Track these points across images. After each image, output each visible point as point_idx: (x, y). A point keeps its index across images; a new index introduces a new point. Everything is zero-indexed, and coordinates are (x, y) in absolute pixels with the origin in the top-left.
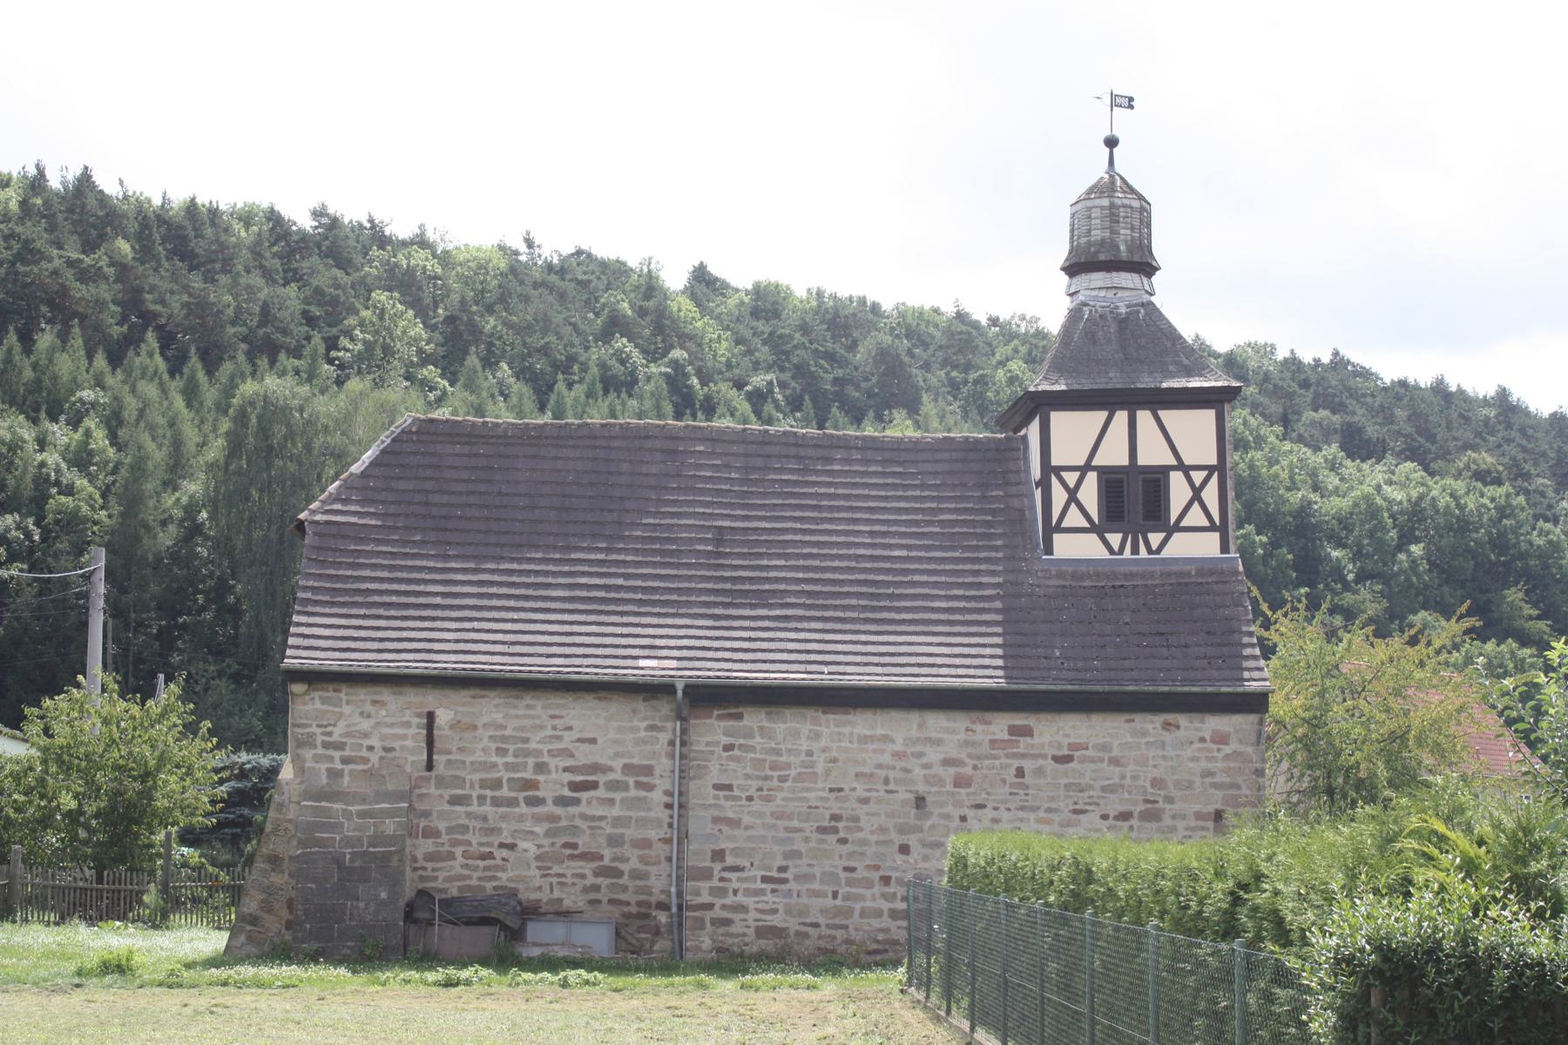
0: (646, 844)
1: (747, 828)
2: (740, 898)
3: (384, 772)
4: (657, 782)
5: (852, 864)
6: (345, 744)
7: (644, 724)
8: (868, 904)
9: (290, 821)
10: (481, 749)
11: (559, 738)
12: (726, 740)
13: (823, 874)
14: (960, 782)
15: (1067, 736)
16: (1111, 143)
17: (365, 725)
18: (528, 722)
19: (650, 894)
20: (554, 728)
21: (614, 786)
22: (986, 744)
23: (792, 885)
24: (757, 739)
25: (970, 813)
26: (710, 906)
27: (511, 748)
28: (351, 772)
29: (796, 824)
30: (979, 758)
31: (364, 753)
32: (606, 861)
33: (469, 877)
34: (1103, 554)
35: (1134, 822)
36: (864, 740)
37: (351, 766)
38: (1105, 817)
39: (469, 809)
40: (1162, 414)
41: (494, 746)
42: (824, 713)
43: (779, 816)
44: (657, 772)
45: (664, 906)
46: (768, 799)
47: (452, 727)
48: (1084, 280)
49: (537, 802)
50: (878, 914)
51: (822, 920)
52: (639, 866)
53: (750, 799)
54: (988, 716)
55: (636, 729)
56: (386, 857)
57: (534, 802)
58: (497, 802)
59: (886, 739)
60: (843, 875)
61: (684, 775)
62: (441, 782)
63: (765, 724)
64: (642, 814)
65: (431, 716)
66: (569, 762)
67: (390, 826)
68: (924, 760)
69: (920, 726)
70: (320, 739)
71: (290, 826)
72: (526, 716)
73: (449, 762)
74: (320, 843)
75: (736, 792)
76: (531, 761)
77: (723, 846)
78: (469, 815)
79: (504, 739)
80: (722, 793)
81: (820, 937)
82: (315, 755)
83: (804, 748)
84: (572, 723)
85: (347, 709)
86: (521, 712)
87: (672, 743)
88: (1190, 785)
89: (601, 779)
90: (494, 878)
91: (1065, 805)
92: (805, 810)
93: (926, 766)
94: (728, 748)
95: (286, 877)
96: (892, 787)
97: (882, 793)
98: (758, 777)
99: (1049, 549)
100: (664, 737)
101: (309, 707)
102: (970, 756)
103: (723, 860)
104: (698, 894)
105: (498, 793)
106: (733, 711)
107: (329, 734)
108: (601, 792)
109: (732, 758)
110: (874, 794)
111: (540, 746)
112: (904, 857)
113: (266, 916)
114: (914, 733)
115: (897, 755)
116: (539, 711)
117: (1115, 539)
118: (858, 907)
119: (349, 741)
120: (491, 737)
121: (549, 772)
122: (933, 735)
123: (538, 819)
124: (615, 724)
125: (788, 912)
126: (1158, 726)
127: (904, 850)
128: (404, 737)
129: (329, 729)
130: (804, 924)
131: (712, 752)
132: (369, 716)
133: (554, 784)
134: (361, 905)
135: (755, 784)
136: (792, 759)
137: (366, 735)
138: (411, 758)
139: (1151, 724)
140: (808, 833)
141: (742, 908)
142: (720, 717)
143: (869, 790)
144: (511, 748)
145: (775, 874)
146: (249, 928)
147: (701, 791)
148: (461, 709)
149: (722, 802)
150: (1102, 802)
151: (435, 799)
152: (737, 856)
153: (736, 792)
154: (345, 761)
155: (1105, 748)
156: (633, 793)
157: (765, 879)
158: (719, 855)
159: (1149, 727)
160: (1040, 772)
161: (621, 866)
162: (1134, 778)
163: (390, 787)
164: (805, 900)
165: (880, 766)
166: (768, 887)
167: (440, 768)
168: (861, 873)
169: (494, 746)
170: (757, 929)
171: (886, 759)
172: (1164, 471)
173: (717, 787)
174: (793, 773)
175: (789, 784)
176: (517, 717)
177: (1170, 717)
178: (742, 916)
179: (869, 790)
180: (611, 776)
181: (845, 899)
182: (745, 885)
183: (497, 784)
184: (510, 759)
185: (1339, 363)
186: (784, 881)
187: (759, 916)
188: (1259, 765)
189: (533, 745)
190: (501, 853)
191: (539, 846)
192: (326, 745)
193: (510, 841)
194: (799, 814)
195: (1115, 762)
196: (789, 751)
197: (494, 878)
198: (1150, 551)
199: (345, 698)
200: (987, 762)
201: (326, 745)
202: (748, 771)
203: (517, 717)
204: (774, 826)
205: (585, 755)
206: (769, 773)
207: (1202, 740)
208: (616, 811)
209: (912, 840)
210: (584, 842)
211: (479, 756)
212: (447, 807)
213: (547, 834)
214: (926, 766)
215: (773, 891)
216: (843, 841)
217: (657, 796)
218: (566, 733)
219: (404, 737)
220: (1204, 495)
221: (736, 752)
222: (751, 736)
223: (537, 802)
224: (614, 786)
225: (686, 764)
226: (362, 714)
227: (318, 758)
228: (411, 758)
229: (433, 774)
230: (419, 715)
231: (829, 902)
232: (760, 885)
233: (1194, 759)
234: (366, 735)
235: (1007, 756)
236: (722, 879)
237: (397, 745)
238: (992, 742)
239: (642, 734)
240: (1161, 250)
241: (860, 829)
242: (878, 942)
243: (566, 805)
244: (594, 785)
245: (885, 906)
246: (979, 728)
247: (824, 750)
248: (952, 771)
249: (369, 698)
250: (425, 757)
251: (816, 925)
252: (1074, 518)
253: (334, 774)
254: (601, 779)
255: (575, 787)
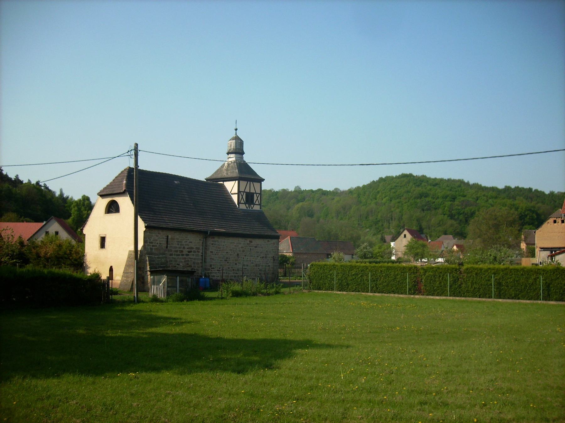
0: (198, 263)
17: (157, 238)
49: (183, 255)
57: (183, 255)
58: (177, 255)
59: (234, 243)
61: (206, 249)
79: (178, 242)
89: (192, 250)
100: (201, 242)
108: (192, 253)
117: (247, 205)
133: (185, 252)
137: (157, 240)
139: (266, 240)
147: (208, 252)
158: (211, 265)
172: (253, 193)
183: (177, 251)
190: (177, 266)
201: (150, 242)
211: (175, 245)
217: (200, 254)
224: (194, 252)
225: (206, 248)
227: (148, 245)
234: (157, 240)
240: (245, 150)
253: (151, 249)
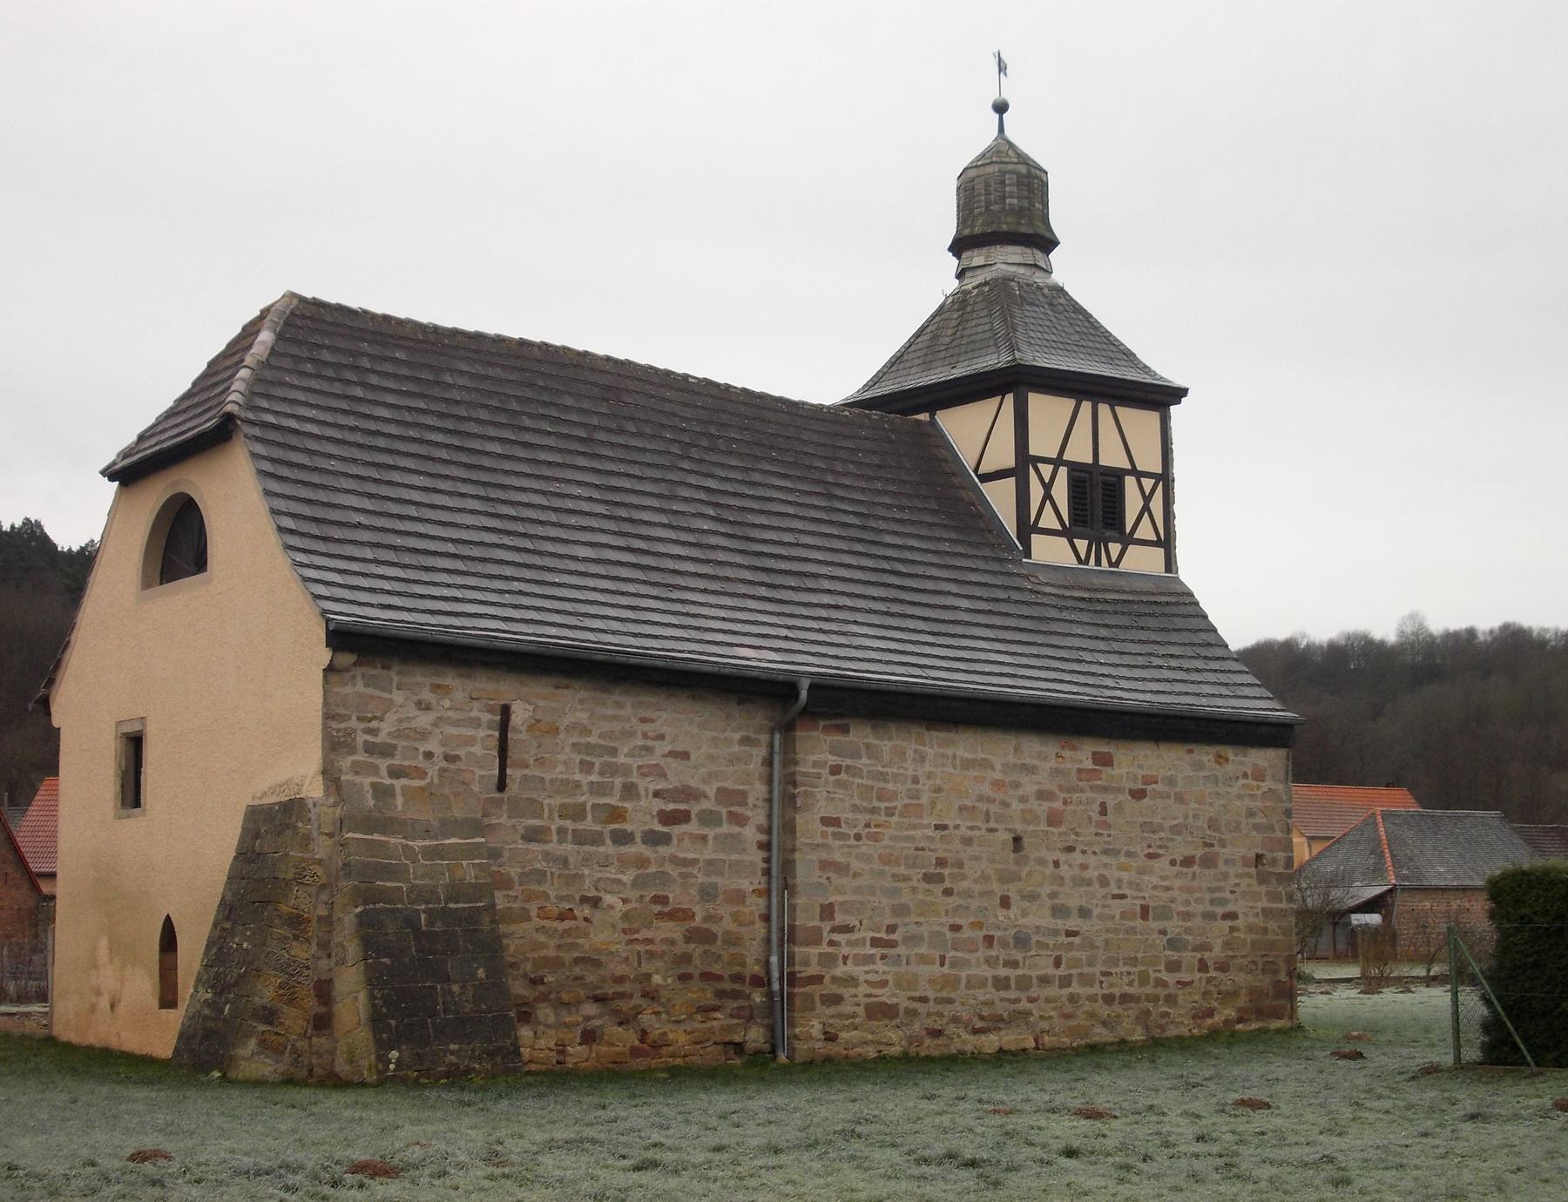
0: (738, 897)
1: (855, 875)
2: (851, 969)
3: (446, 791)
4: (749, 814)
5: (959, 921)
6: (394, 747)
7: (737, 736)
8: (973, 971)
9: (320, 862)
10: (563, 762)
11: (650, 750)
12: (833, 760)
13: (932, 934)
14: (1054, 819)
15: (1140, 767)
16: (1001, 108)
18: (617, 727)
19: (743, 964)
20: (645, 736)
21: (709, 818)
22: (1074, 776)
23: (901, 950)
24: (865, 760)
25: (1062, 857)
26: (818, 979)
27: (597, 761)
28: (404, 788)
29: (902, 870)
30: (1069, 790)
31: (420, 762)
32: (698, 921)
33: (544, 946)
34: (1071, 561)
35: (1196, 868)
36: (967, 764)
37: (404, 781)
38: (1173, 863)
39: (548, 847)
40: (1118, 409)
41: (578, 758)
42: (928, 729)
43: (886, 860)
44: (751, 800)
45: (757, 981)
46: (875, 838)
47: (530, 729)
48: (977, 258)
49: (623, 838)
50: (982, 983)
51: (931, 994)
52: (733, 927)
53: (858, 837)
54: (1075, 741)
55: (729, 742)
56: (472, 916)
58: (580, 838)
59: (986, 764)
60: (949, 935)
62: (516, 810)
63: (871, 740)
64: (735, 857)
65: (506, 711)
66: (661, 785)
67: (469, 871)
68: (1021, 792)
69: (1016, 750)
70: (361, 738)
71: (319, 871)
72: (615, 717)
73: (525, 778)
74: (382, 895)
75: (844, 829)
76: (618, 781)
77: (832, 899)
78: (546, 854)
79: (590, 749)
80: (830, 830)
81: (929, 1015)
82: (354, 763)
83: (910, 773)
84: (664, 730)
85: (398, 697)
86: (609, 712)
87: (769, 762)
88: (1237, 828)
89: (695, 809)
90: (574, 946)
91: (1140, 849)
92: (912, 852)
93: (1023, 799)
94: (836, 770)
95: (314, 948)
96: (992, 825)
97: (983, 832)
98: (866, 810)
99: (1028, 554)
100: (759, 753)
101: (348, 690)
102: (1061, 789)
103: (831, 917)
104: (807, 964)
105: (580, 826)
106: (839, 722)
107: (374, 732)
108: (693, 827)
109: (839, 784)
110: (977, 833)
111: (629, 761)
112: (1005, 912)
113: (285, 1009)
114: (1011, 759)
115: (998, 785)
116: (628, 711)
117: (1081, 545)
118: (964, 974)
119: (402, 743)
120: (574, 745)
121: (638, 797)
122: (1028, 761)
123: (624, 863)
124: (709, 734)
125: (898, 985)
126: (1211, 757)
127: (1005, 902)
128: (471, 741)
129: (374, 724)
130: (913, 999)
131: (819, 776)
132: (428, 708)
133: (642, 815)
134: (456, 988)
135: (863, 818)
136: (900, 787)
137: (423, 735)
138: (479, 772)
140: (914, 883)
141: (852, 981)
142: (827, 729)
143: (971, 828)
144: (597, 761)
145: (883, 935)
146: (262, 1028)
147: (808, 824)
148: (542, 703)
149: (830, 840)
150: (1170, 844)
151: (507, 828)
152: (846, 912)
153: (844, 829)
154: (395, 773)
155: (1171, 782)
156: (726, 828)
157: (876, 942)
158: (827, 911)
159: (1205, 759)
160: (1119, 808)
161: (713, 928)
162: (1196, 816)
163: (458, 813)
164: (914, 968)
165: (980, 798)
166: (878, 952)
167: (513, 787)
168: (967, 933)
169: (578, 758)
170: (867, 1007)
171: (986, 789)
173: (826, 821)
174: (899, 804)
175: (895, 819)
176: (605, 718)
177: (1221, 749)
178: (852, 991)
179: (971, 828)
180: (705, 805)
181: (952, 966)
182: (855, 951)
183: (578, 813)
184: (594, 778)
185: (27, 521)
186: (892, 944)
187: (870, 990)
188: (1287, 805)
189: (621, 759)
191: (625, 901)
192: (370, 749)
193: (593, 893)
194: (907, 858)
195: (1180, 798)
196: (896, 776)
197: (574, 946)
198: (1111, 564)
199: (396, 679)
200: (1075, 796)
201: (370, 749)
202: (857, 801)
203: (605, 718)
204: (882, 873)
205: (678, 776)
206: (877, 804)
207: (1245, 776)
208: (708, 853)
209: (1012, 890)
210: (677, 896)
211: (559, 772)
212: (521, 845)
213: (636, 883)
214: (1023, 799)
215: (883, 957)
216: (948, 892)
217: (751, 834)
218: (657, 744)
219: (471, 741)
220: (1152, 505)
221: (843, 776)
222: (857, 755)
223: (623, 838)
224: (709, 818)
225: (786, 794)
226: (419, 704)
227: (357, 769)
228: (479, 772)
229: (505, 796)
230: (490, 710)
231: (936, 969)
232: (869, 950)
233: (1240, 797)
234: (423, 735)
235: (1092, 788)
236: (831, 943)
237: (461, 752)
238: (1080, 771)
239: (737, 748)
241: (963, 877)
242: (982, 1018)
243: (657, 844)
244: (684, 817)
245: (988, 973)
246: (1067, 753)
247: (930, 776)
248: (1046, 805)
249: (428, 681)
250: (496, 772)
251: (924, 1000)
252: (1049, 520)
254: (695, 809)
255: (669, 818)
